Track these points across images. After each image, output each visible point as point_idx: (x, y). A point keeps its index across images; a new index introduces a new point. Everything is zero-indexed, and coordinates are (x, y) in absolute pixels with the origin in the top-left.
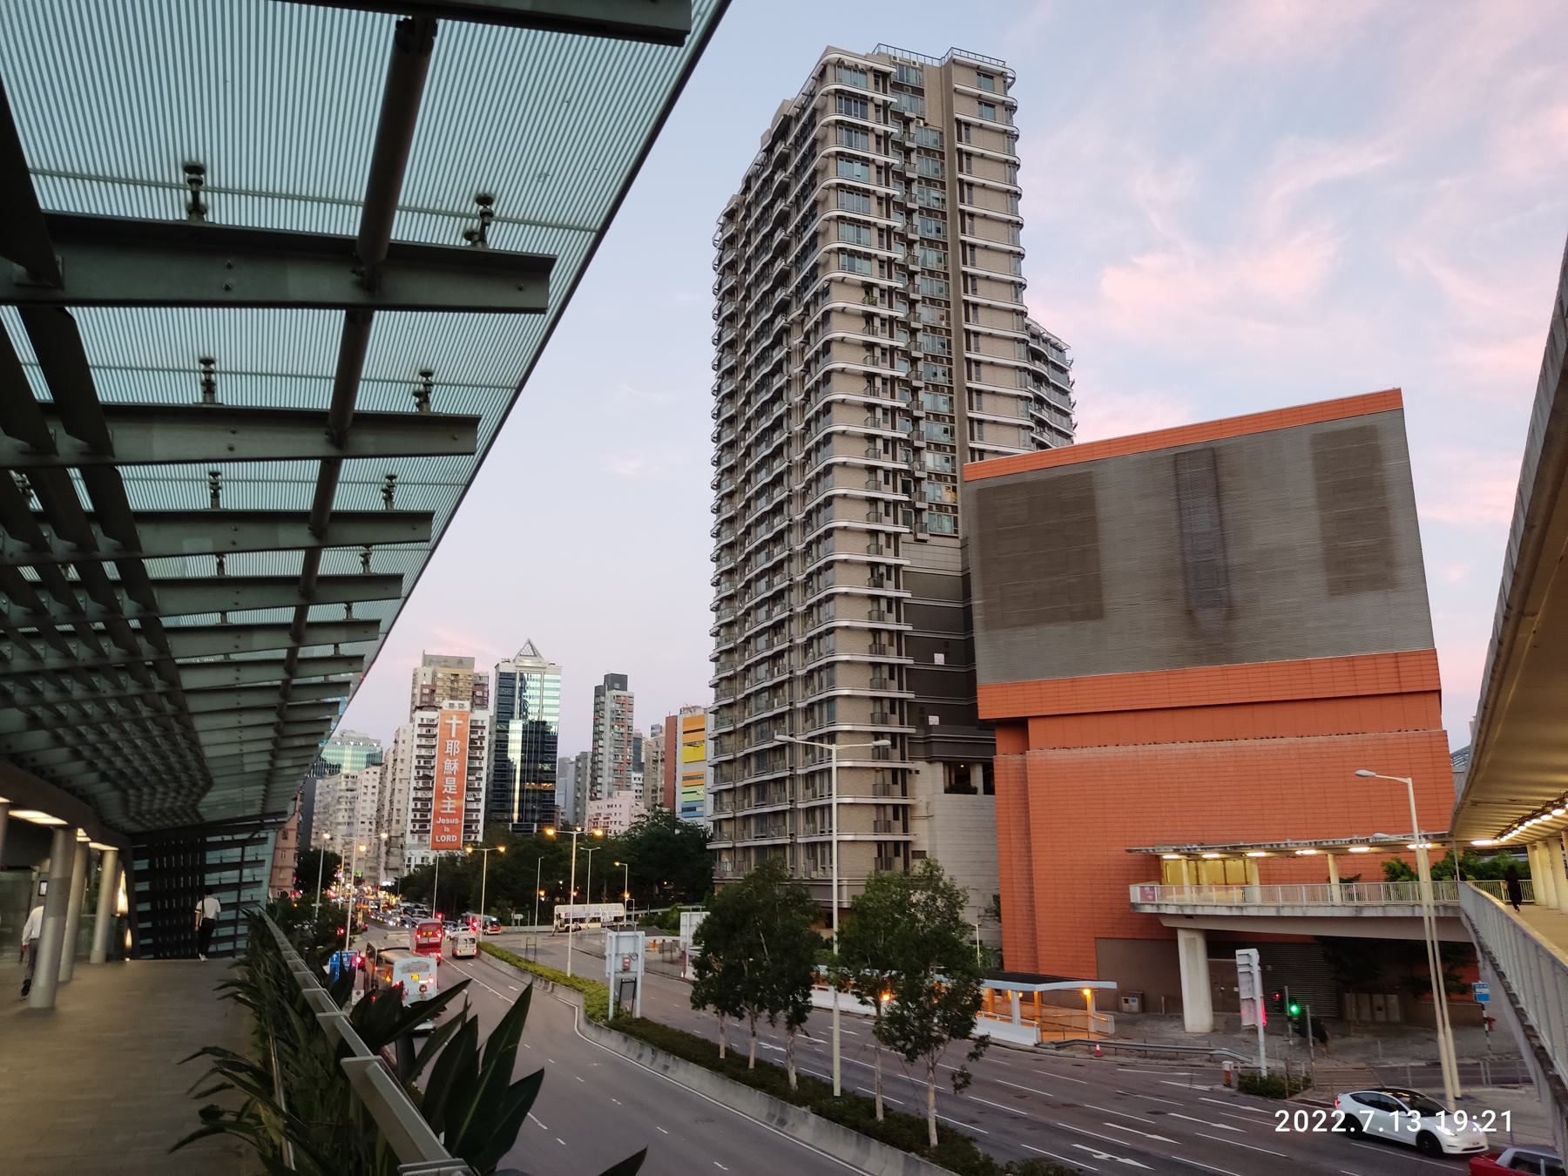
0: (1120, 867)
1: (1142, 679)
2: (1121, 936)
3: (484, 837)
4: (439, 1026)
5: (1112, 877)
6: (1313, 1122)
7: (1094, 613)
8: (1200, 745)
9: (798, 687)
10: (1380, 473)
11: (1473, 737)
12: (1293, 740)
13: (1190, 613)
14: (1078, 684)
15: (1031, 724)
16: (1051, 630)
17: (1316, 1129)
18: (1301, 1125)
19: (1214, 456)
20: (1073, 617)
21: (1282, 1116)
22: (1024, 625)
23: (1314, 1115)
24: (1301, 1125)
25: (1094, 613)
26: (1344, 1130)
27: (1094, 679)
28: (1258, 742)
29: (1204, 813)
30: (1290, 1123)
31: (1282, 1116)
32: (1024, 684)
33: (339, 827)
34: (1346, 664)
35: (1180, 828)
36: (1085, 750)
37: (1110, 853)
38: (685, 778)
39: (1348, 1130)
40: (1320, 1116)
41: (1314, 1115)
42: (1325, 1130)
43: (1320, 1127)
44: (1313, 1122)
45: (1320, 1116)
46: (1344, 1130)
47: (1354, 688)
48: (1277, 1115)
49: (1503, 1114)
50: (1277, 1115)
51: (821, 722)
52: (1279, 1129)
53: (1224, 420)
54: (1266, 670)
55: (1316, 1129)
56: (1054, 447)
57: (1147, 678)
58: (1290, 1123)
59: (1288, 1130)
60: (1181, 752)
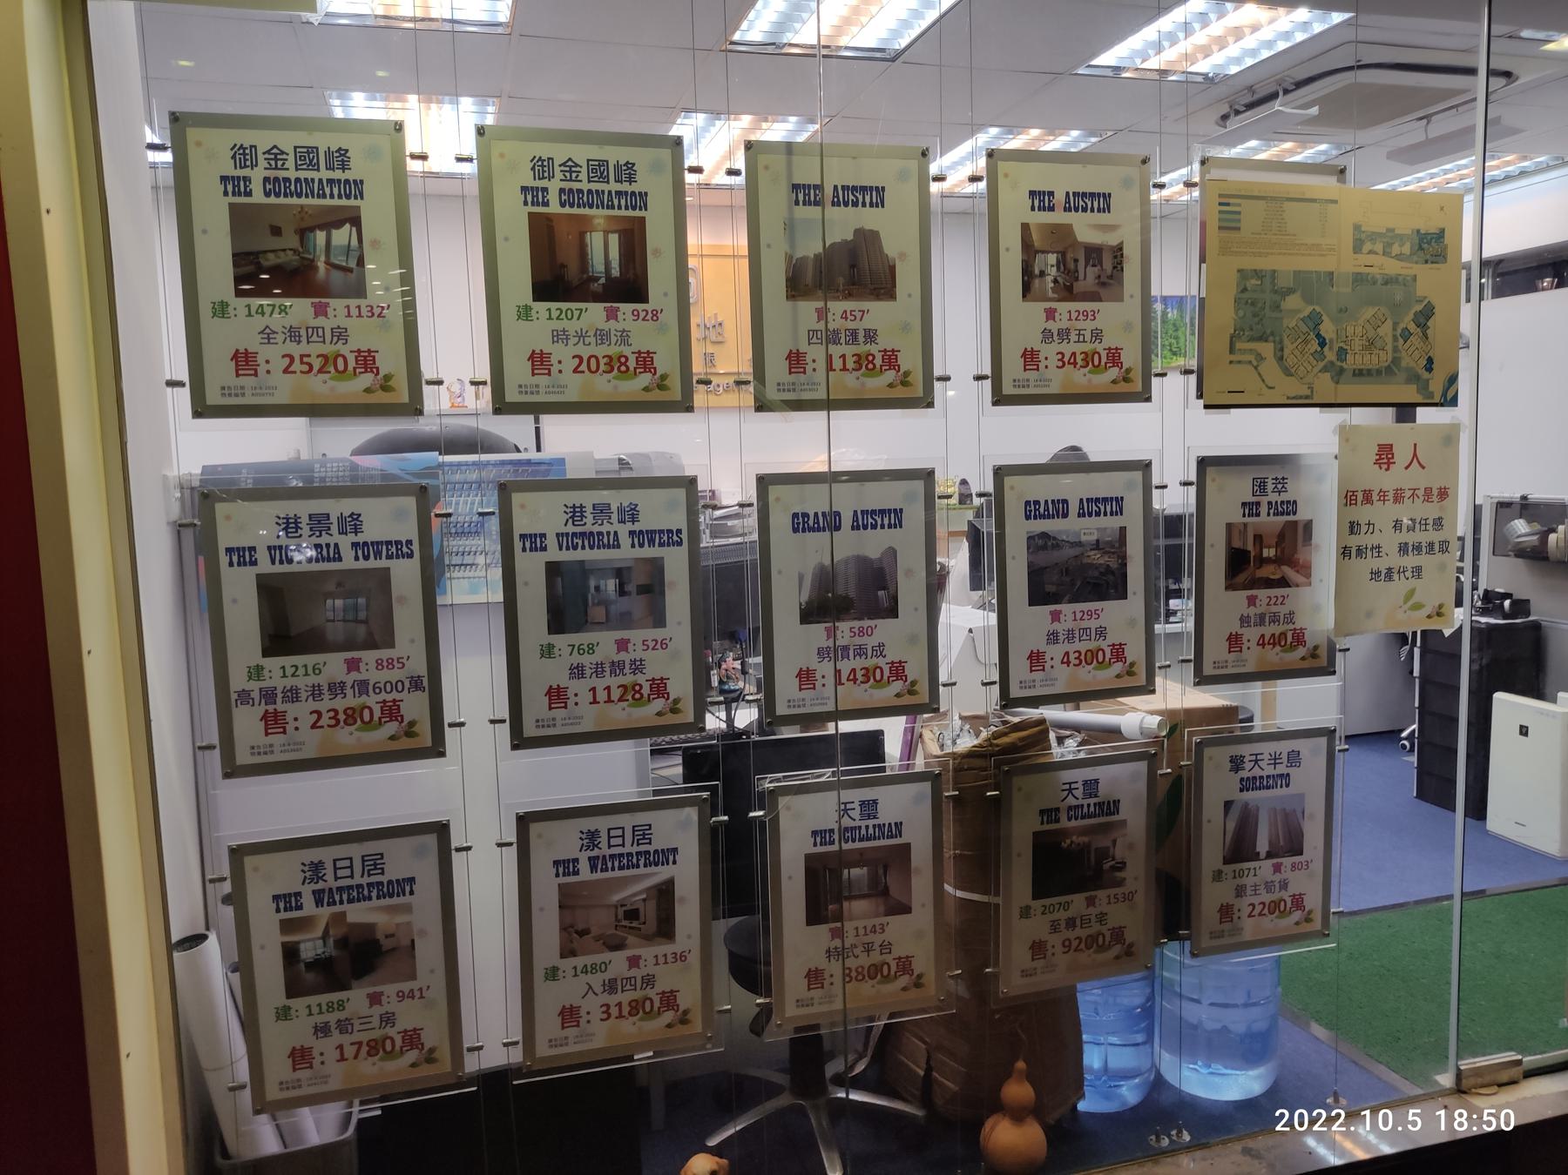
3: (674, 735)
4: (1329, 1153)
10: (1397, 371)
11: (1173, 9)
21: (1282, 1115)
23: (1314, 1114)
26: (1344, 1129)
31: (1282, 1115)
33: (1238, 1021)
39: (1348, 1129)
40: (1320, 1115)
41: (1314, 1114)
43: (1339, 1126)
44: (1313, 1122)
45: (1320, 1115)
46: (1344, 1129)
48: (1277, 1114)
49: (1438, 1113)
50: (1277, 1114)
55: (1316, 1128)
56: (1415, 726)
58: (1290, 1123)
59: (1288, 1129)
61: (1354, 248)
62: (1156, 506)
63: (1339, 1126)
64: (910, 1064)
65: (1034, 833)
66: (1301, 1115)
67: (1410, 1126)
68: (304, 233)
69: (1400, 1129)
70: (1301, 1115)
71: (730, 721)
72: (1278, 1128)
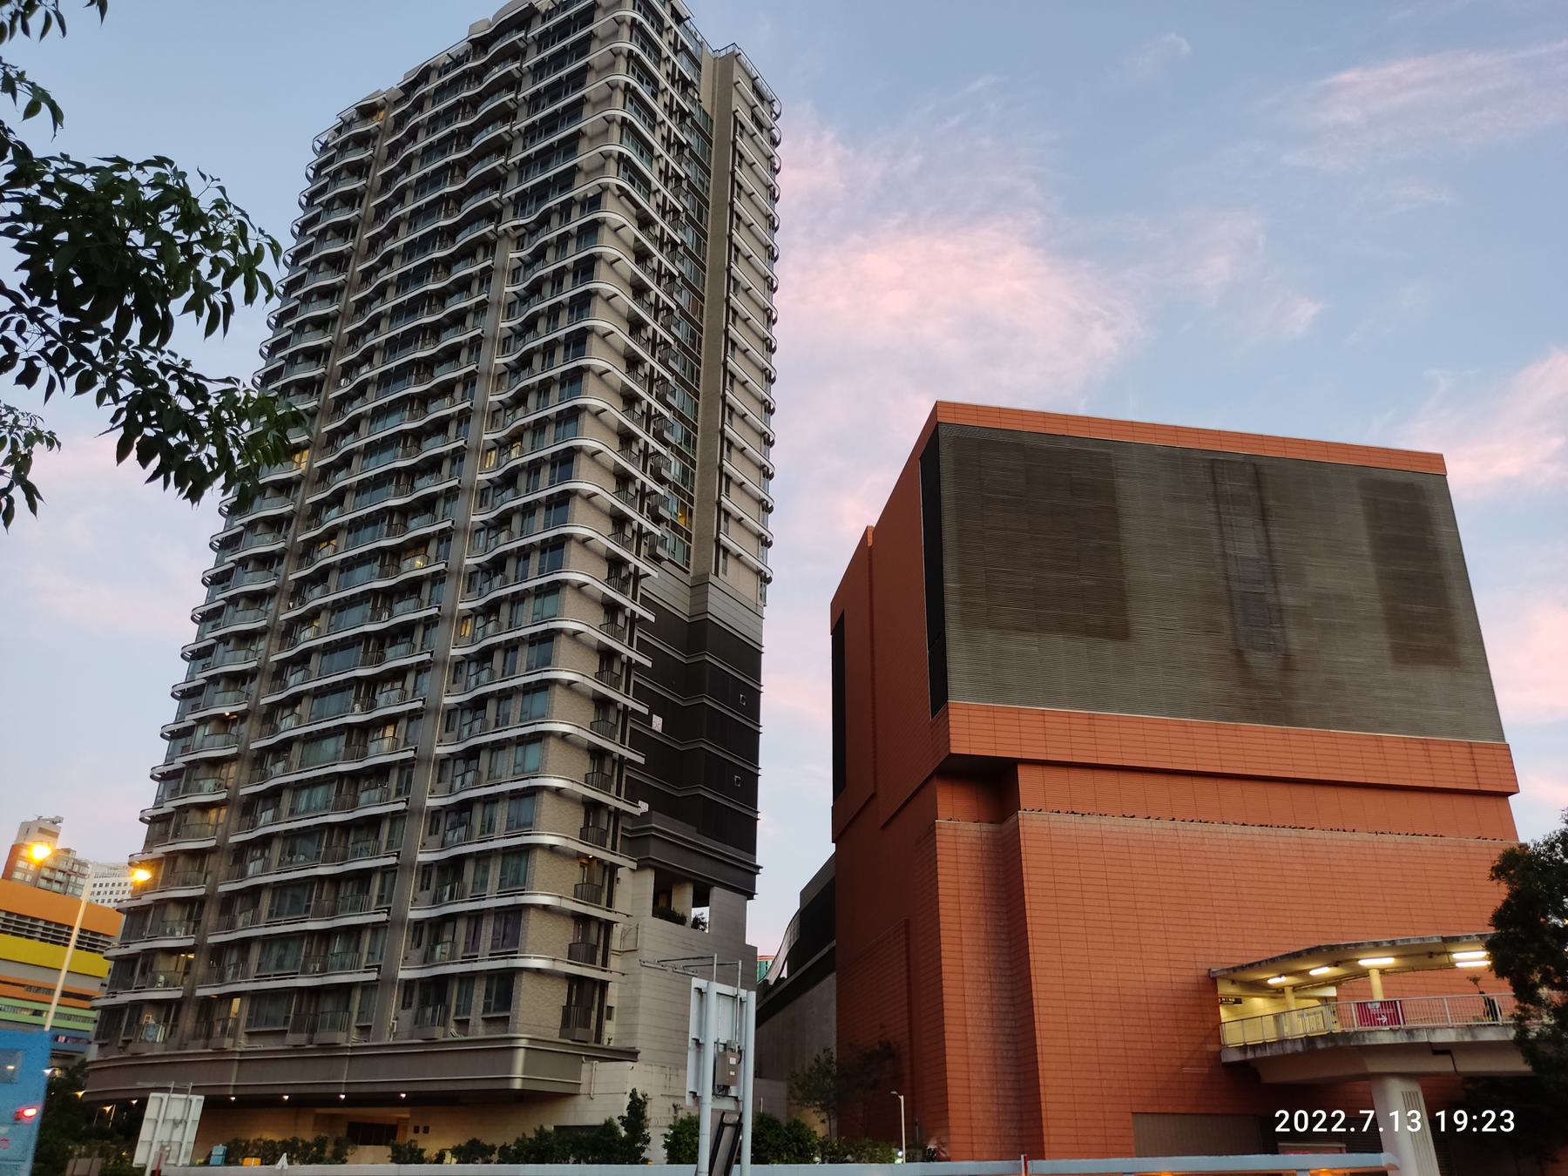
0: (1163, 1000)
1: (1183, 729)
2: (1170, 1109)
5: (1153, 1015)
6: (1313, 1122)
7: (1119, 631)
8: (1256, 830)
9: (419, 829)
12: (1366, 836)
13: (1239, 653)
14: (1096, 722)
15: (1025, 776)
16: (1058, 642)
17: (1316, 1129)
18: (1301, 1125)
19: (1257, 473)
20: (1088, 631)
21: (1282, 1116)
22: (1020, 629)
23: (1314, 1115)
24: (1301, 1125)
25: (1119, 631)
27: (1119, 719)
28: (1328, 834)
29: (1270, 926)
30: (1290, 1124)
31: (1282, 1116)
32: (1019, 712)
34: (1420, 746)
35: (1241, 946)
36: (1104, 820)
37: (1148, 978)
38: (64, 994)
39: (1348, 1130)
40: (1320, 1116)
41: (1314, 1115)
42: (1325, 1130)
43: (1339, 1127)
44: (1313, 1122)
47: (1431, 778)
48: (1277, 1115)
49: (1437, 1114)
50: (1277, 1115)
51: (475, 946)
52: (1278, 1129)
53: (1412, 452)
54: (1333, 740)
55: (1316, 1129)
57: (1190, 730)
58: (1290, 1124)
59: (1288, 1130)
60: (1235, 837)
61: (678, 923)
62: (152, 1095)
63: (1339, 1127)
64: (126, 1017)
65: (1442, 455)
66: (1301, 1117)
67: (1502, 1128)
68: (30, 440)
69: (1475, 1130)
70: (1301, 1117)
71: (35, 227)
72: (1278, 1129)
